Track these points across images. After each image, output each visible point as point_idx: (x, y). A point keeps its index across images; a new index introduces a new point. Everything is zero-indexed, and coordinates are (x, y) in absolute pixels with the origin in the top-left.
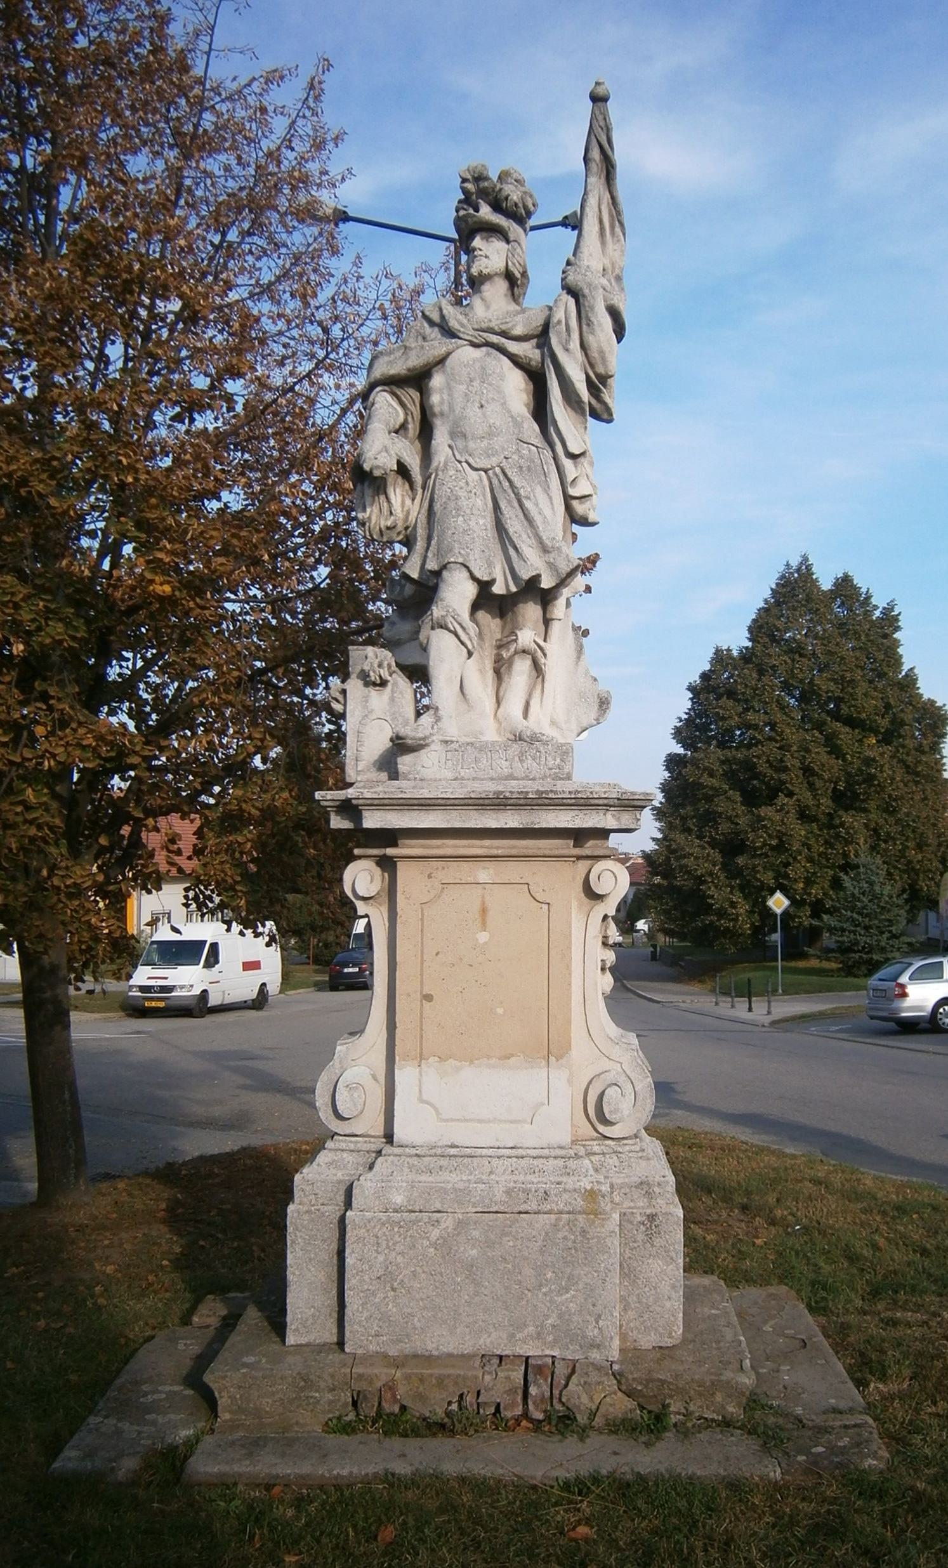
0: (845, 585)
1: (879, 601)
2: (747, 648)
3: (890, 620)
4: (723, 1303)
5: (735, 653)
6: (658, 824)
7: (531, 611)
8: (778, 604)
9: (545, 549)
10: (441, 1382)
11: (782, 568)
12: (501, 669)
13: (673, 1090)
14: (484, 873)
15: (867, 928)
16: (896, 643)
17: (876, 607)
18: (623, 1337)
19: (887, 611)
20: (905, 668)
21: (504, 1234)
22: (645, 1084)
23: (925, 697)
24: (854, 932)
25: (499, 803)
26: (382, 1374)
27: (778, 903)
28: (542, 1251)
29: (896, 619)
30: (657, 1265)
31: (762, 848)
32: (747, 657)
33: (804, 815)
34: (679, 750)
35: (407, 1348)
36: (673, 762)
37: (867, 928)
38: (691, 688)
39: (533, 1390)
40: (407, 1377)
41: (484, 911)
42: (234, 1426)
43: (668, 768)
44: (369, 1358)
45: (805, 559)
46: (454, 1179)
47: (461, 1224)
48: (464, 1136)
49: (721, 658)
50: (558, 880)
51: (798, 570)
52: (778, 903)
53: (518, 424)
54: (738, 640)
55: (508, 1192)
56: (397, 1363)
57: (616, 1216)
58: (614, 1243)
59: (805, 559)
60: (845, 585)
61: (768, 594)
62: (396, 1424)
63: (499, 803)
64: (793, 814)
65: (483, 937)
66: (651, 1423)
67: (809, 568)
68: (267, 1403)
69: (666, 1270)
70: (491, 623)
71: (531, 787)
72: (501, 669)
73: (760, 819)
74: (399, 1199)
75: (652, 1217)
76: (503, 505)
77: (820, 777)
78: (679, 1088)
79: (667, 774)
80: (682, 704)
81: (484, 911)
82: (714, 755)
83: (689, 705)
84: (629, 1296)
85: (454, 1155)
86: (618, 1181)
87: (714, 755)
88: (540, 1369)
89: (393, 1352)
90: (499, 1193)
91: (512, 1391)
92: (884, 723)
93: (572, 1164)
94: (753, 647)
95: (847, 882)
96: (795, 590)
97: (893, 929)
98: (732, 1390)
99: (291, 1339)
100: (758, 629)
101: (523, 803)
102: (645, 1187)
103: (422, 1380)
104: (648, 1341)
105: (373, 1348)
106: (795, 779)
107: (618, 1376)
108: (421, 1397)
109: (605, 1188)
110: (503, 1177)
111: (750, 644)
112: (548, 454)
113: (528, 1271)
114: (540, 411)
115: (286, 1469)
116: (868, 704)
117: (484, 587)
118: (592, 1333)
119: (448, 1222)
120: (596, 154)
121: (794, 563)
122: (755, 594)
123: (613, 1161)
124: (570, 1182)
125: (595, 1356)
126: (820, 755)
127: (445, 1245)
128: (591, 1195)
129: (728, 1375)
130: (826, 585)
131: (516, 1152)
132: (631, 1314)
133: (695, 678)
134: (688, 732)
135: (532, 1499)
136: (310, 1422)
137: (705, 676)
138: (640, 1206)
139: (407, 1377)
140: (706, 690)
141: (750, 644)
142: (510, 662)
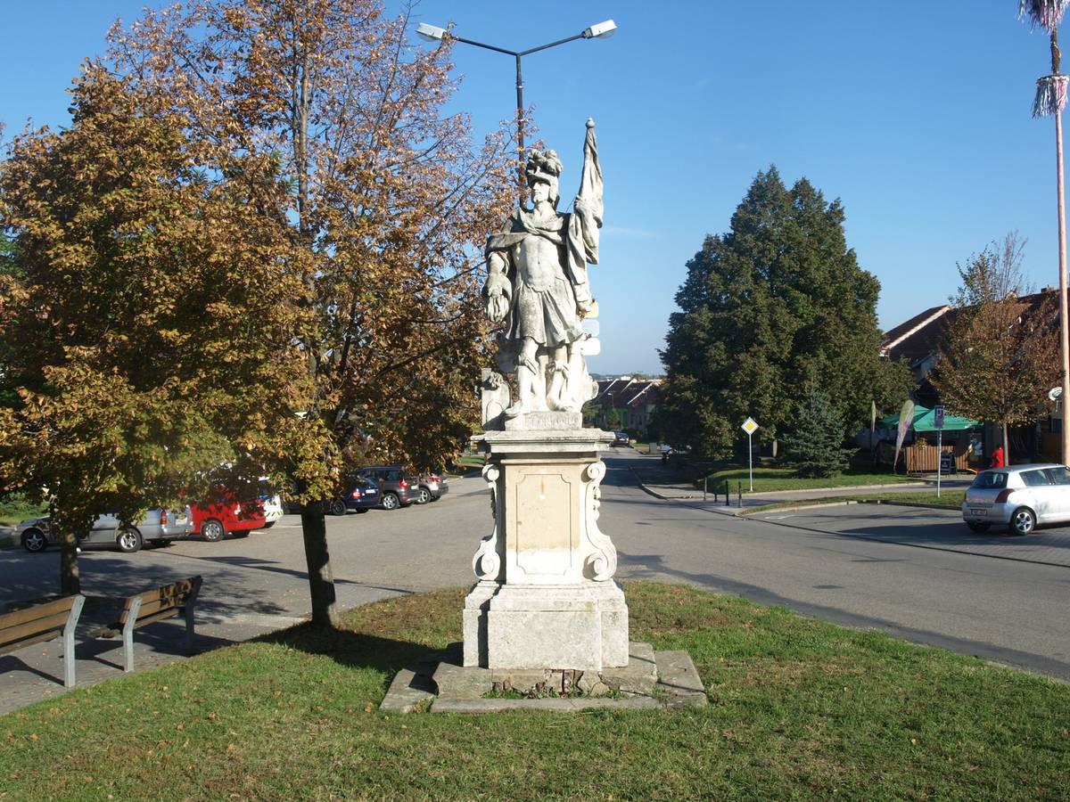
0: (803, 189)
1: (829, 199)
2: (730, 235)
3: (836, 214)
4: (646, 650)
5: (721, 239)
6: (665, 366)
7: (562, 352)
8: (752, 202)
9: (566, 326)
10: (528, 679)
11: (756, 175)
12: (549, 378)
13: (660, 561)
14: (543, 470)
15: (816, 443)
16: (840, 230)
17: (826, 204)
18: (604, 663)
19: (833, 207)
20: (848, 248)
21: (553, 620)
22: (613, 557)
23: (863, 270)
24: (807, 447)
25: (548, 442)
26: (505, 676)
27: (750, 426)
28: (569, 626)
29: (841, 212)
30: (617, 633)
31: (740, 384)
32: (729, 240)
33: (771, 359)
34: (680, 310)
35: (514, 666)
36: (675, 319)
37: (816, 443)
38: (689, 265)
39: (566, 682)
40: (515, 677)
41: (543, 486)
42: (445, 696)
43: (672, 324)
44: (498, 670)
45: (773, 169)
46: (531, 598)
47: (536, 616)
48: (536, 580)
49: (710, 243)
50: (573, 472)
51: (768, 176)
52: (750, 426)
53: (555, 270)
54: (723, 228)
55: (555, 603)
56: (511, 671)
57: (600, 613)
58: (599, 624)
59: (773, 169)
60: (803, 189)
61: (745, 194)
62: (513, 693)
63: (548, 442)
64: (763, 359)
65: (542, 497)
66: (614, 694)
67: (776, 175)
68: (458, 687)
69: (621, 634)
70: (544, 359)
71: (562, 435)
72: (549, 378)
73: (738, 362)
74: (510, 606)
75: (615, 613)
76: (548, 308)
77: (783, 331)
78: (663, 559)
79: (671, 328)
80: (681, 277)
81: (543, 486)
82: (705, 316)
83: (687, 277)
84: (605, 646)
85: (532, 588)
86: (601, 598)
87: (705, 316)
88: (568, 674)
89: (508, 667)
90: (551, 603)
91: (557, 682)
92: (831, 291)
93: (581, 591)
94: (735, 234)
95: (802, 410)
96: (763, 192)
97: (835, 444)
98: (649, 682)
99: (465, 664)
100: (736, 221)
101: (558, 442)
102: (612, 601)
103: (521, 678)
104: (614, 664)
105: (500, 667)
106: (766, 335)
107: (600, 677)
108: (521, 685)
109: (595, 601)
110: (551, 599)
111: (732, 232)
112: (568, 282)
113: (564, 635)
114: (564, 262)
115: (470, 708)
116: (818, 275)
117: (541, 345)
118: (590, 660)
119: (530, 615)
120: (589, 150)
121: (765, 171)
122: (738, 194)
123: (598, 590)
124: (580, 599)
125: (591, 669)
126: (782, 314)
127: (529, 625)
128: (589, 604)
129: (646, 676)
130: (789, 187)
131: (557, 587)
132: (607, 653)
133: (692, 257)
134: (687, 297)
135: (565, 719)
136: (475, 694)
137: (699, 256)
138: (611, 609)
139: (515, 677)
140: (700, 265)
141: (732, 232)
142: (552, 376)
